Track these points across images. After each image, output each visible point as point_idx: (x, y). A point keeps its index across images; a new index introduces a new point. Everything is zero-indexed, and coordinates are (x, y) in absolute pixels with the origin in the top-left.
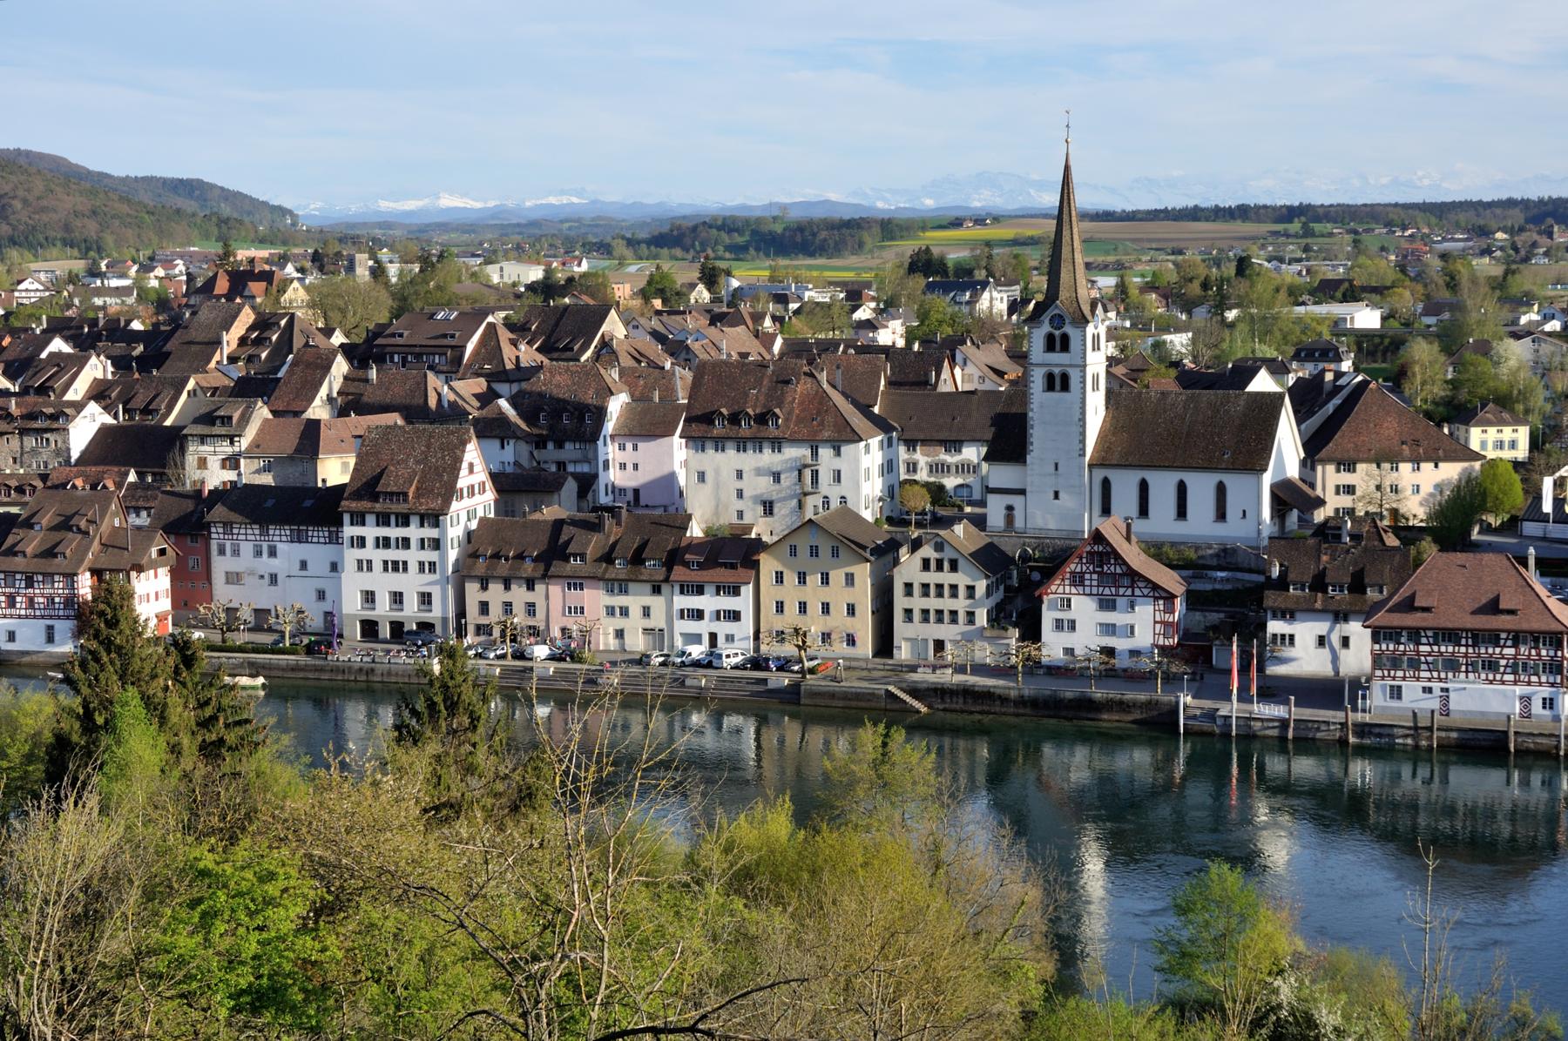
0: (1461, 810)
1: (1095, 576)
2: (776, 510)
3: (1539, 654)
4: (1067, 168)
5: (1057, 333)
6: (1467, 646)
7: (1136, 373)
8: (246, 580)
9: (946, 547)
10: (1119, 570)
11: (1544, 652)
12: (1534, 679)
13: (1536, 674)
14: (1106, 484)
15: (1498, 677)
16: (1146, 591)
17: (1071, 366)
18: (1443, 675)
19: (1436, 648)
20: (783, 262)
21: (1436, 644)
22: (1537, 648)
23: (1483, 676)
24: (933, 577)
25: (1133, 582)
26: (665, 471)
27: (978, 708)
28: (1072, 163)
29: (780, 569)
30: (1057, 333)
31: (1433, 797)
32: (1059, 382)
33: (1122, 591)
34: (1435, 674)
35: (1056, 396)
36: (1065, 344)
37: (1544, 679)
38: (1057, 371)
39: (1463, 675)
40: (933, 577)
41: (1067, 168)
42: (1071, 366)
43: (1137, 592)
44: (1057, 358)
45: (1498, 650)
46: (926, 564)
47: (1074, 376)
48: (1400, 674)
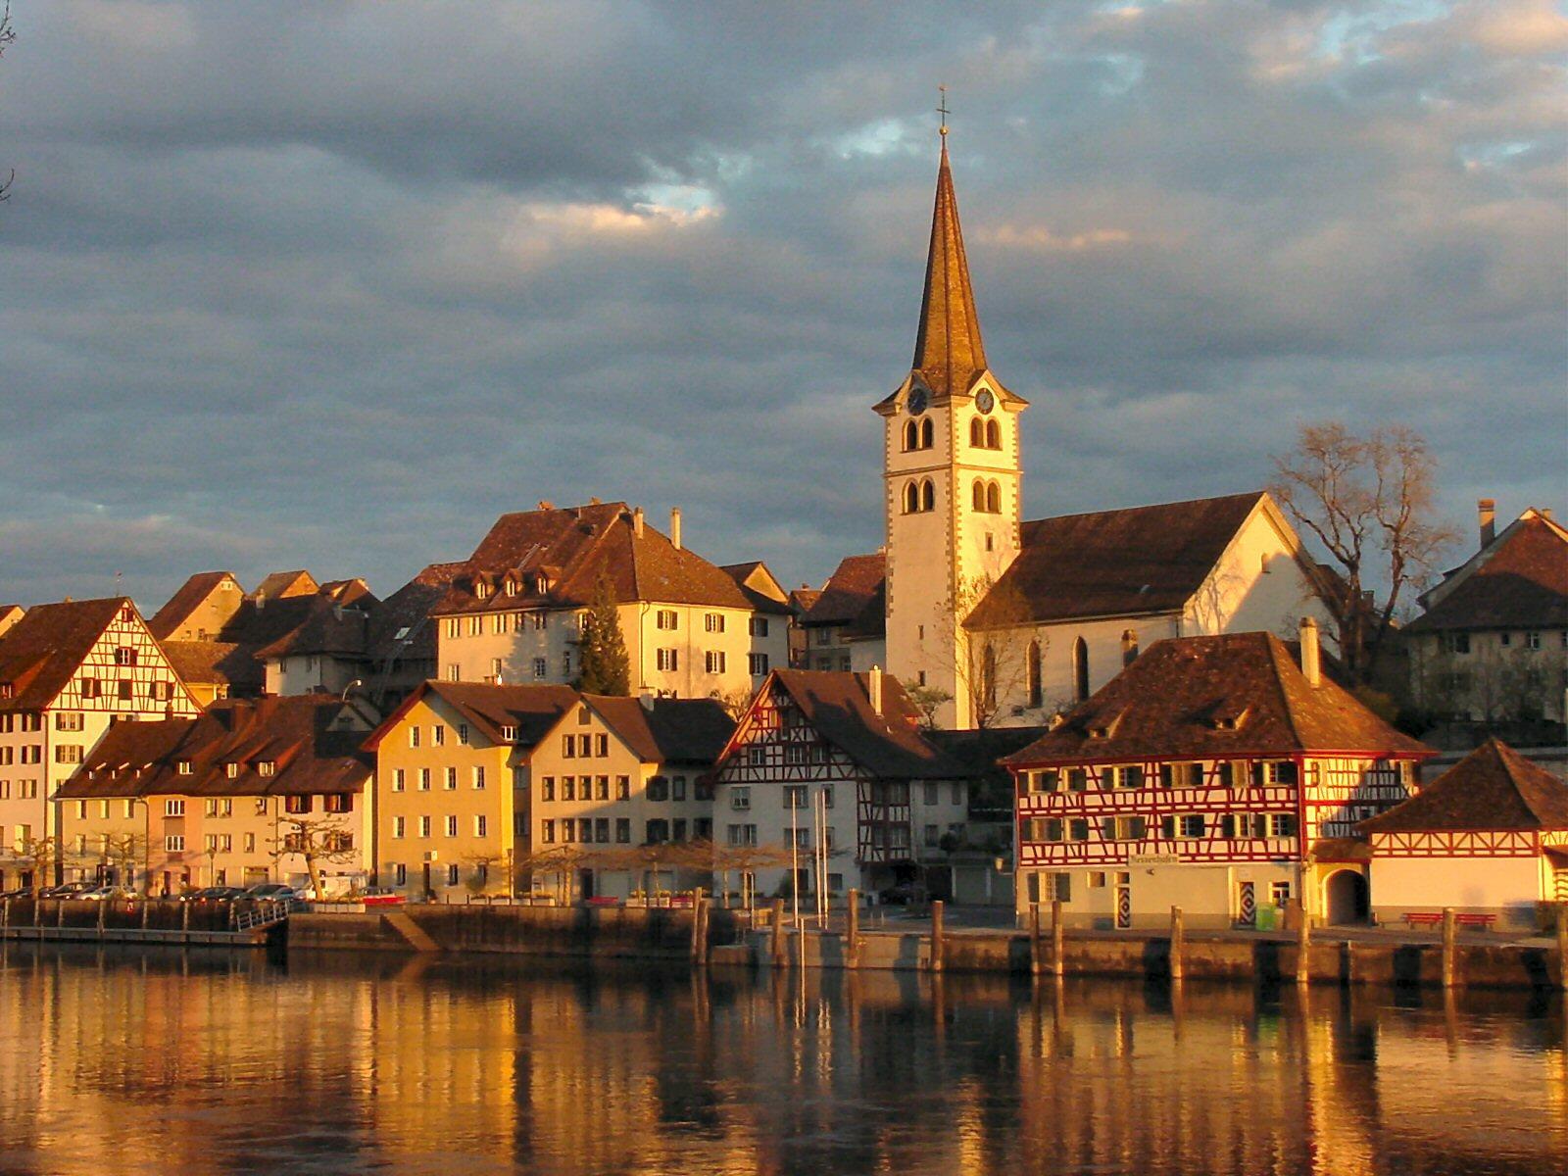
0: (987, 1095)
2: (678, 803)
5: (985, 418)
6: (1154, 790)
11: (1270, 795)
14: (989, 651)
16: (846, 770)
18: (1122, 851)
20: (1243, 591)
24: (578, 767)
26: (708, 816)
27: (216, 951)
30: (917, 418)
32: (923, 497)
33: (815, 770)
34: (1110, 848)
38: (919, 478)
39: (1151, 846)
43: (835, 773)
44: (921, 458)
45: (1200, 795)
47: (939, 481)
48: (1059, 851)
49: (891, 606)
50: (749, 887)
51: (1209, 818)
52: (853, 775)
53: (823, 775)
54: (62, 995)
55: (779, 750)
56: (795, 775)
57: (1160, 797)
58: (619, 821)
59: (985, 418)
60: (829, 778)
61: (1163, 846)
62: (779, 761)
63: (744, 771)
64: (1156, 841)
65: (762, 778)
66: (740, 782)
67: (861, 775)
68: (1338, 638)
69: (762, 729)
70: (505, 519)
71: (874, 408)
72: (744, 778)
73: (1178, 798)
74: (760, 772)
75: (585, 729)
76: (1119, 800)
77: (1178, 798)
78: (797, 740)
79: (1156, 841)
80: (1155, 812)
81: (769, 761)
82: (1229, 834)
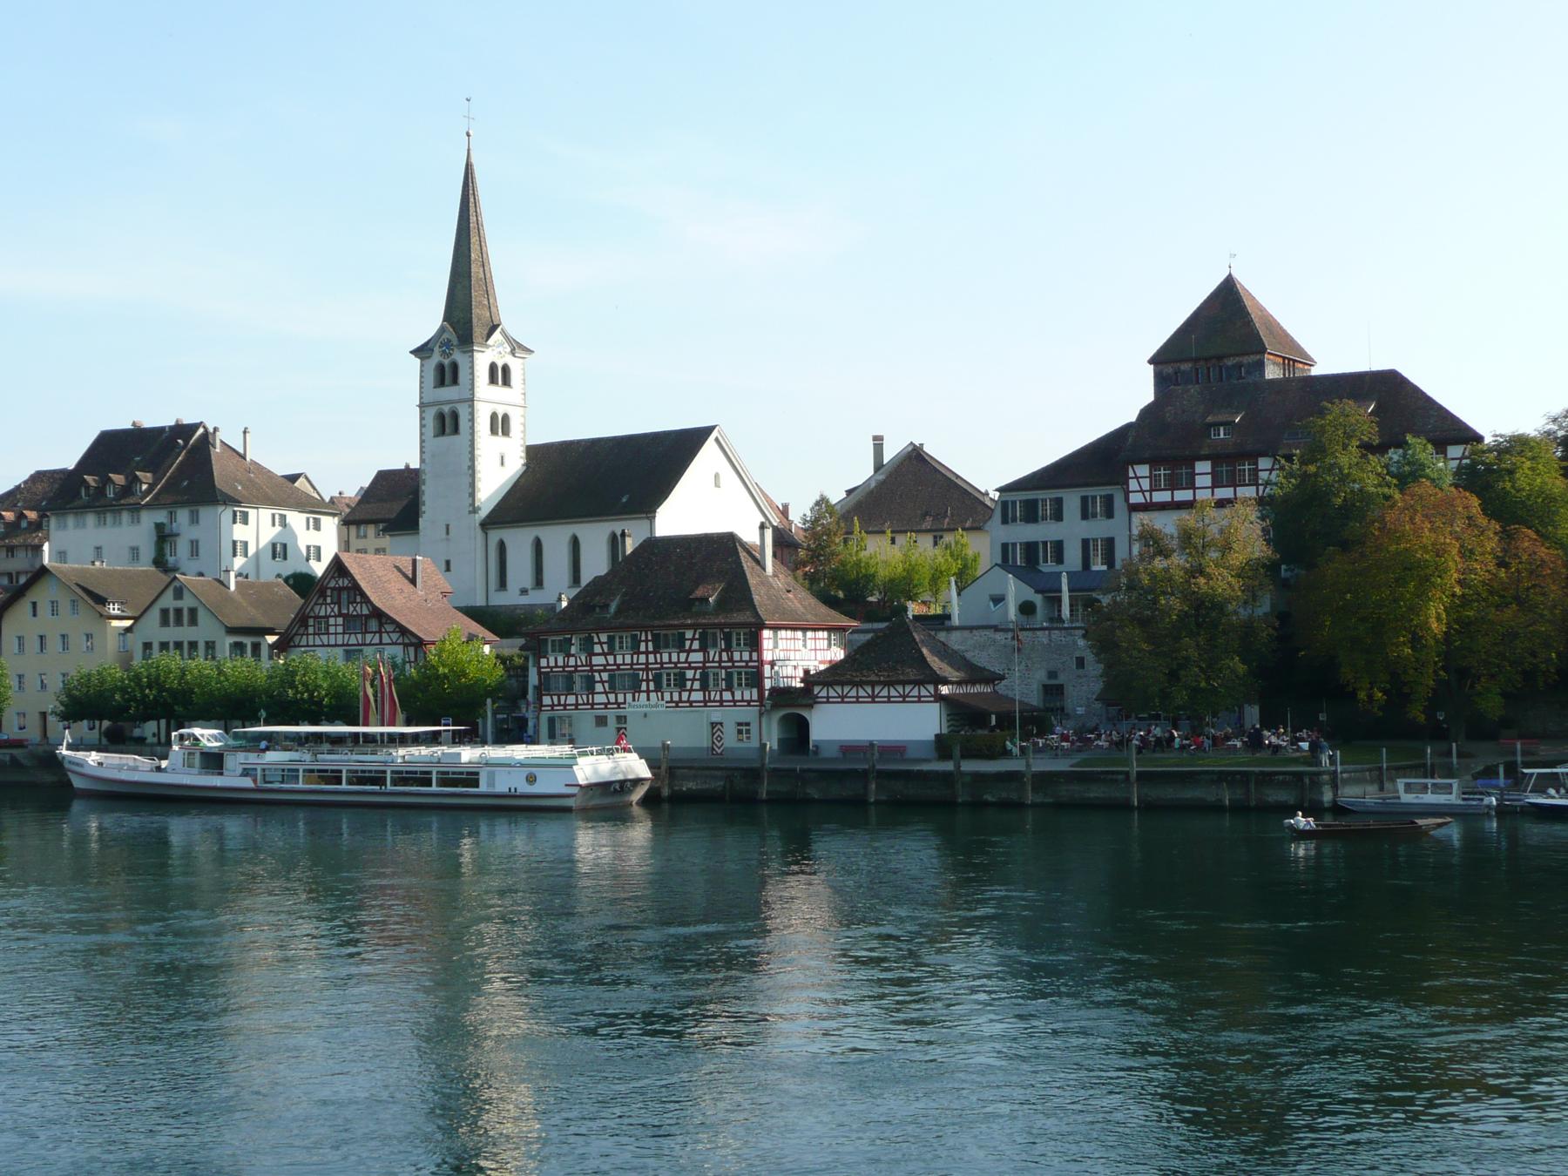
1: (340, 621)
3: (731, 660)
4: (469, 169)
5: (446, 362)
6: (647, 653)
7: (1532, 449)
8: (240, 771)
9: (186, 594)
10: (365, 612)
11: (736, 656)
12: (727, 696)
13: (730, 688)
15: (685, 696)
17: (460, 401)
18: (621, 698)
19: (611, 659)
21: (611, 652)
22: (728, 649)
23: (667, 696)
24: (172, 634)
25: (381, 625)
28: (473, 160)
31: (467, 842)
33: (369, 637)
37: (738, 696)
38: (446, 409)
40: (172, 634)
41: (469, 169)
42: (460, 401)
43: (386, 639)
45: (683, 656)
47: (463, 411)
48: (571, 699)
51: (690, 674)
53: (377, 640)
55: (340, 621)
56: (353, 640)
57: (651, 657)
61: (653, 695)
62: (340, 629)
64: (648, 691)
73: (666, 658)
74: (325, 638)
75: (179, 604)
76: (619, 660)
77: (666, 658)
79: (648, 691)
80: (647, 669)
81: (332, 630)
82: (704, 688)
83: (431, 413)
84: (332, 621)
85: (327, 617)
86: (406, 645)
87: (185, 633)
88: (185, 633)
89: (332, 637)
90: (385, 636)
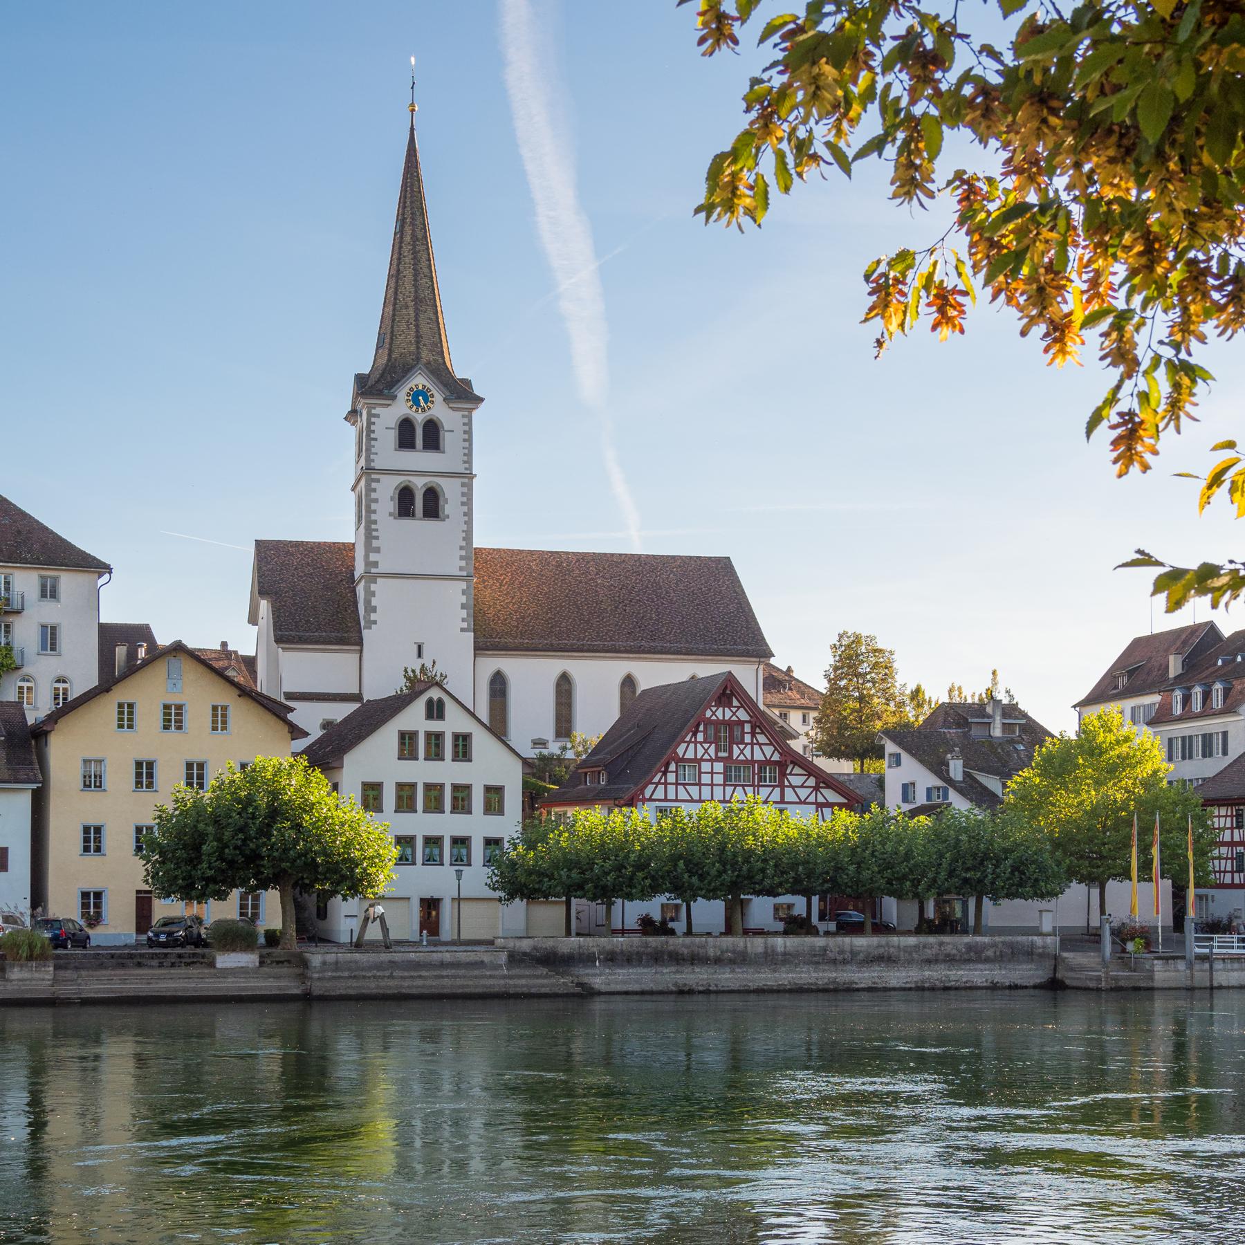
5: (419, 418)
16: (803, 793)
24: (421, 772)
29: (220, 702)
35: (418, 526)
36: (433, 437)
38: (419, 484)
40: (421, 772)
46: (407, 742)
47: (451, 489)
49: (464, 613)
50: (1232, 947)
52: (812, 799)
54: (267, 1009)
55: (719, 767)
58: (400, 786)
59: (419, 418)
60: (782, 801)
62: (719, 779)
63: (671, 789)
65: (696, 797)
66: (666, 800)
67: (821, 799)
68: (485, 720)
69: (696, 743)
70: (721, 569)
71: (1005, 18)
72: (671, 796)
74: (694, 791)
75: (435, 726)
78: (741, 757)
81: (706, 779)
83: (387, 489)
84: (706, 767)
85: (698, 761)
86: (820, 806)
87: (447, 772)
88: (447, 772)
89: (706, 791)
90: (788, 791)
